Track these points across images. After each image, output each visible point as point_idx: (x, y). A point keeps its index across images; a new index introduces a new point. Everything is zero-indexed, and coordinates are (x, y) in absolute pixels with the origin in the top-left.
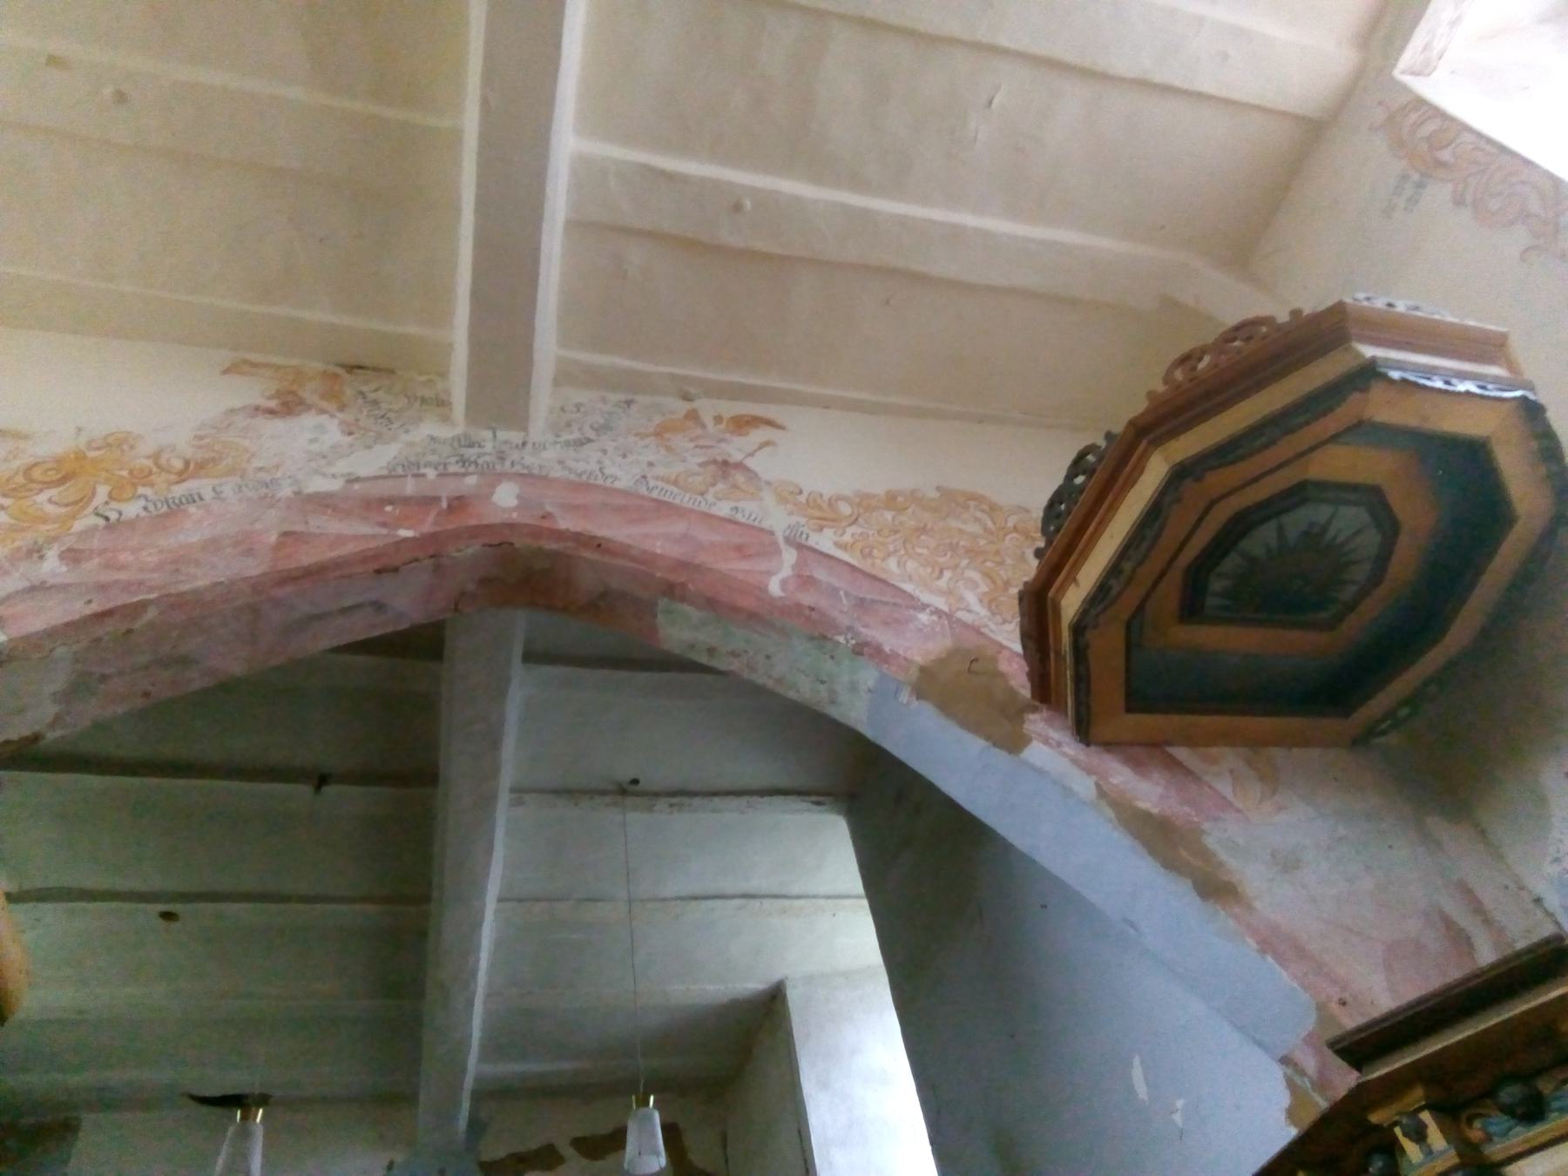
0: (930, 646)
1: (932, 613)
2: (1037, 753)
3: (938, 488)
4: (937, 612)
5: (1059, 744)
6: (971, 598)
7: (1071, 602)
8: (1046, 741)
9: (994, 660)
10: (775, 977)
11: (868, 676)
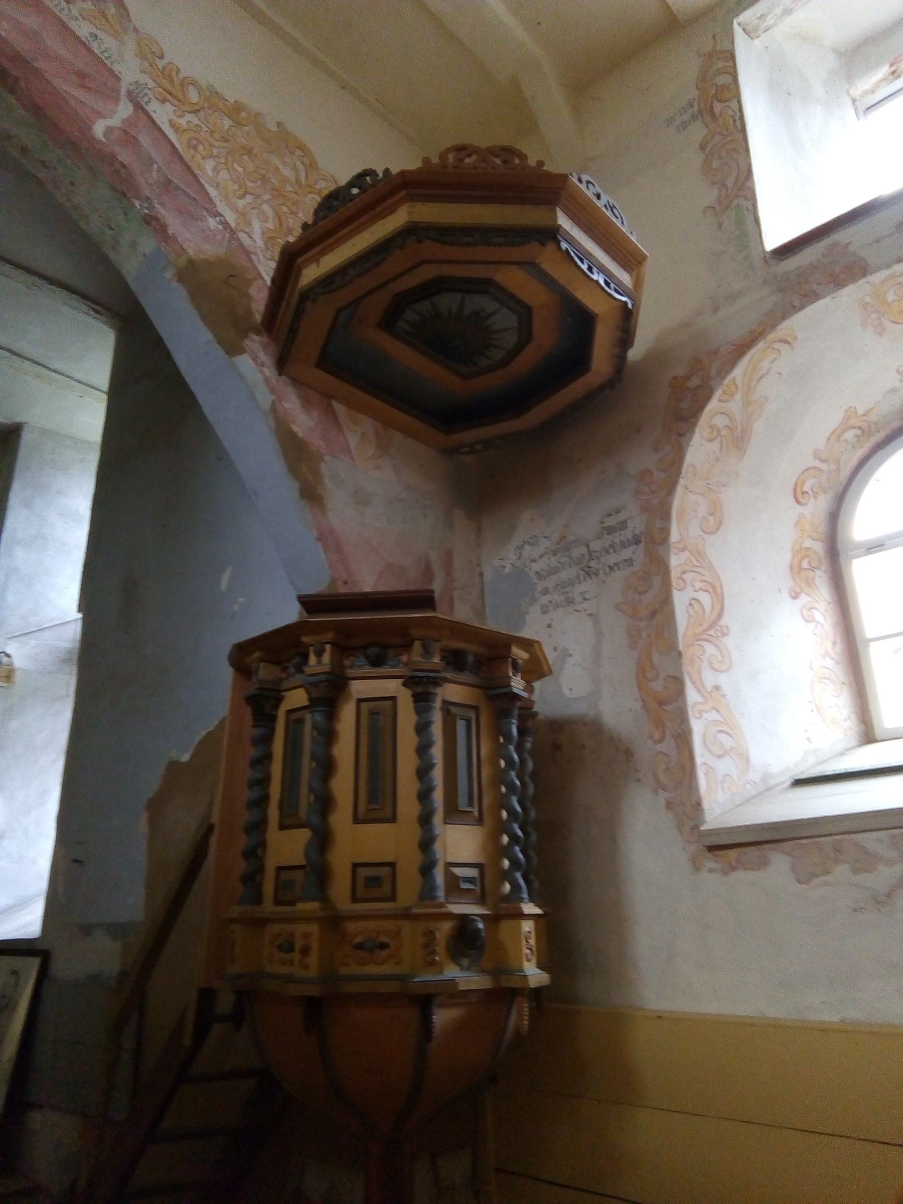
0: (206, 247)
1: (221, 223)
2: (244, 362)
3: (279, 124)
4: (225, 224)
5: (263, 365)
6: (257, 228)
7: (310, 274)
8: (255, 359)
9: (249, 283)
10: (19, 419)
11: (148, 244)
